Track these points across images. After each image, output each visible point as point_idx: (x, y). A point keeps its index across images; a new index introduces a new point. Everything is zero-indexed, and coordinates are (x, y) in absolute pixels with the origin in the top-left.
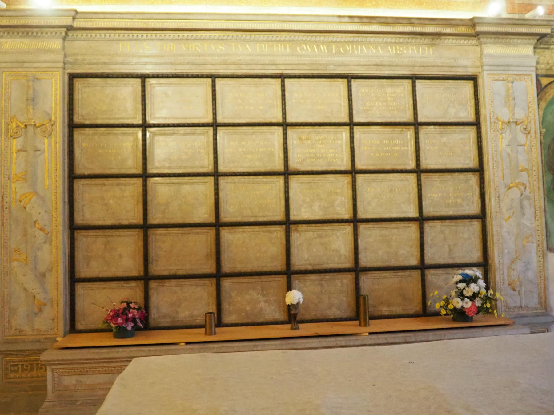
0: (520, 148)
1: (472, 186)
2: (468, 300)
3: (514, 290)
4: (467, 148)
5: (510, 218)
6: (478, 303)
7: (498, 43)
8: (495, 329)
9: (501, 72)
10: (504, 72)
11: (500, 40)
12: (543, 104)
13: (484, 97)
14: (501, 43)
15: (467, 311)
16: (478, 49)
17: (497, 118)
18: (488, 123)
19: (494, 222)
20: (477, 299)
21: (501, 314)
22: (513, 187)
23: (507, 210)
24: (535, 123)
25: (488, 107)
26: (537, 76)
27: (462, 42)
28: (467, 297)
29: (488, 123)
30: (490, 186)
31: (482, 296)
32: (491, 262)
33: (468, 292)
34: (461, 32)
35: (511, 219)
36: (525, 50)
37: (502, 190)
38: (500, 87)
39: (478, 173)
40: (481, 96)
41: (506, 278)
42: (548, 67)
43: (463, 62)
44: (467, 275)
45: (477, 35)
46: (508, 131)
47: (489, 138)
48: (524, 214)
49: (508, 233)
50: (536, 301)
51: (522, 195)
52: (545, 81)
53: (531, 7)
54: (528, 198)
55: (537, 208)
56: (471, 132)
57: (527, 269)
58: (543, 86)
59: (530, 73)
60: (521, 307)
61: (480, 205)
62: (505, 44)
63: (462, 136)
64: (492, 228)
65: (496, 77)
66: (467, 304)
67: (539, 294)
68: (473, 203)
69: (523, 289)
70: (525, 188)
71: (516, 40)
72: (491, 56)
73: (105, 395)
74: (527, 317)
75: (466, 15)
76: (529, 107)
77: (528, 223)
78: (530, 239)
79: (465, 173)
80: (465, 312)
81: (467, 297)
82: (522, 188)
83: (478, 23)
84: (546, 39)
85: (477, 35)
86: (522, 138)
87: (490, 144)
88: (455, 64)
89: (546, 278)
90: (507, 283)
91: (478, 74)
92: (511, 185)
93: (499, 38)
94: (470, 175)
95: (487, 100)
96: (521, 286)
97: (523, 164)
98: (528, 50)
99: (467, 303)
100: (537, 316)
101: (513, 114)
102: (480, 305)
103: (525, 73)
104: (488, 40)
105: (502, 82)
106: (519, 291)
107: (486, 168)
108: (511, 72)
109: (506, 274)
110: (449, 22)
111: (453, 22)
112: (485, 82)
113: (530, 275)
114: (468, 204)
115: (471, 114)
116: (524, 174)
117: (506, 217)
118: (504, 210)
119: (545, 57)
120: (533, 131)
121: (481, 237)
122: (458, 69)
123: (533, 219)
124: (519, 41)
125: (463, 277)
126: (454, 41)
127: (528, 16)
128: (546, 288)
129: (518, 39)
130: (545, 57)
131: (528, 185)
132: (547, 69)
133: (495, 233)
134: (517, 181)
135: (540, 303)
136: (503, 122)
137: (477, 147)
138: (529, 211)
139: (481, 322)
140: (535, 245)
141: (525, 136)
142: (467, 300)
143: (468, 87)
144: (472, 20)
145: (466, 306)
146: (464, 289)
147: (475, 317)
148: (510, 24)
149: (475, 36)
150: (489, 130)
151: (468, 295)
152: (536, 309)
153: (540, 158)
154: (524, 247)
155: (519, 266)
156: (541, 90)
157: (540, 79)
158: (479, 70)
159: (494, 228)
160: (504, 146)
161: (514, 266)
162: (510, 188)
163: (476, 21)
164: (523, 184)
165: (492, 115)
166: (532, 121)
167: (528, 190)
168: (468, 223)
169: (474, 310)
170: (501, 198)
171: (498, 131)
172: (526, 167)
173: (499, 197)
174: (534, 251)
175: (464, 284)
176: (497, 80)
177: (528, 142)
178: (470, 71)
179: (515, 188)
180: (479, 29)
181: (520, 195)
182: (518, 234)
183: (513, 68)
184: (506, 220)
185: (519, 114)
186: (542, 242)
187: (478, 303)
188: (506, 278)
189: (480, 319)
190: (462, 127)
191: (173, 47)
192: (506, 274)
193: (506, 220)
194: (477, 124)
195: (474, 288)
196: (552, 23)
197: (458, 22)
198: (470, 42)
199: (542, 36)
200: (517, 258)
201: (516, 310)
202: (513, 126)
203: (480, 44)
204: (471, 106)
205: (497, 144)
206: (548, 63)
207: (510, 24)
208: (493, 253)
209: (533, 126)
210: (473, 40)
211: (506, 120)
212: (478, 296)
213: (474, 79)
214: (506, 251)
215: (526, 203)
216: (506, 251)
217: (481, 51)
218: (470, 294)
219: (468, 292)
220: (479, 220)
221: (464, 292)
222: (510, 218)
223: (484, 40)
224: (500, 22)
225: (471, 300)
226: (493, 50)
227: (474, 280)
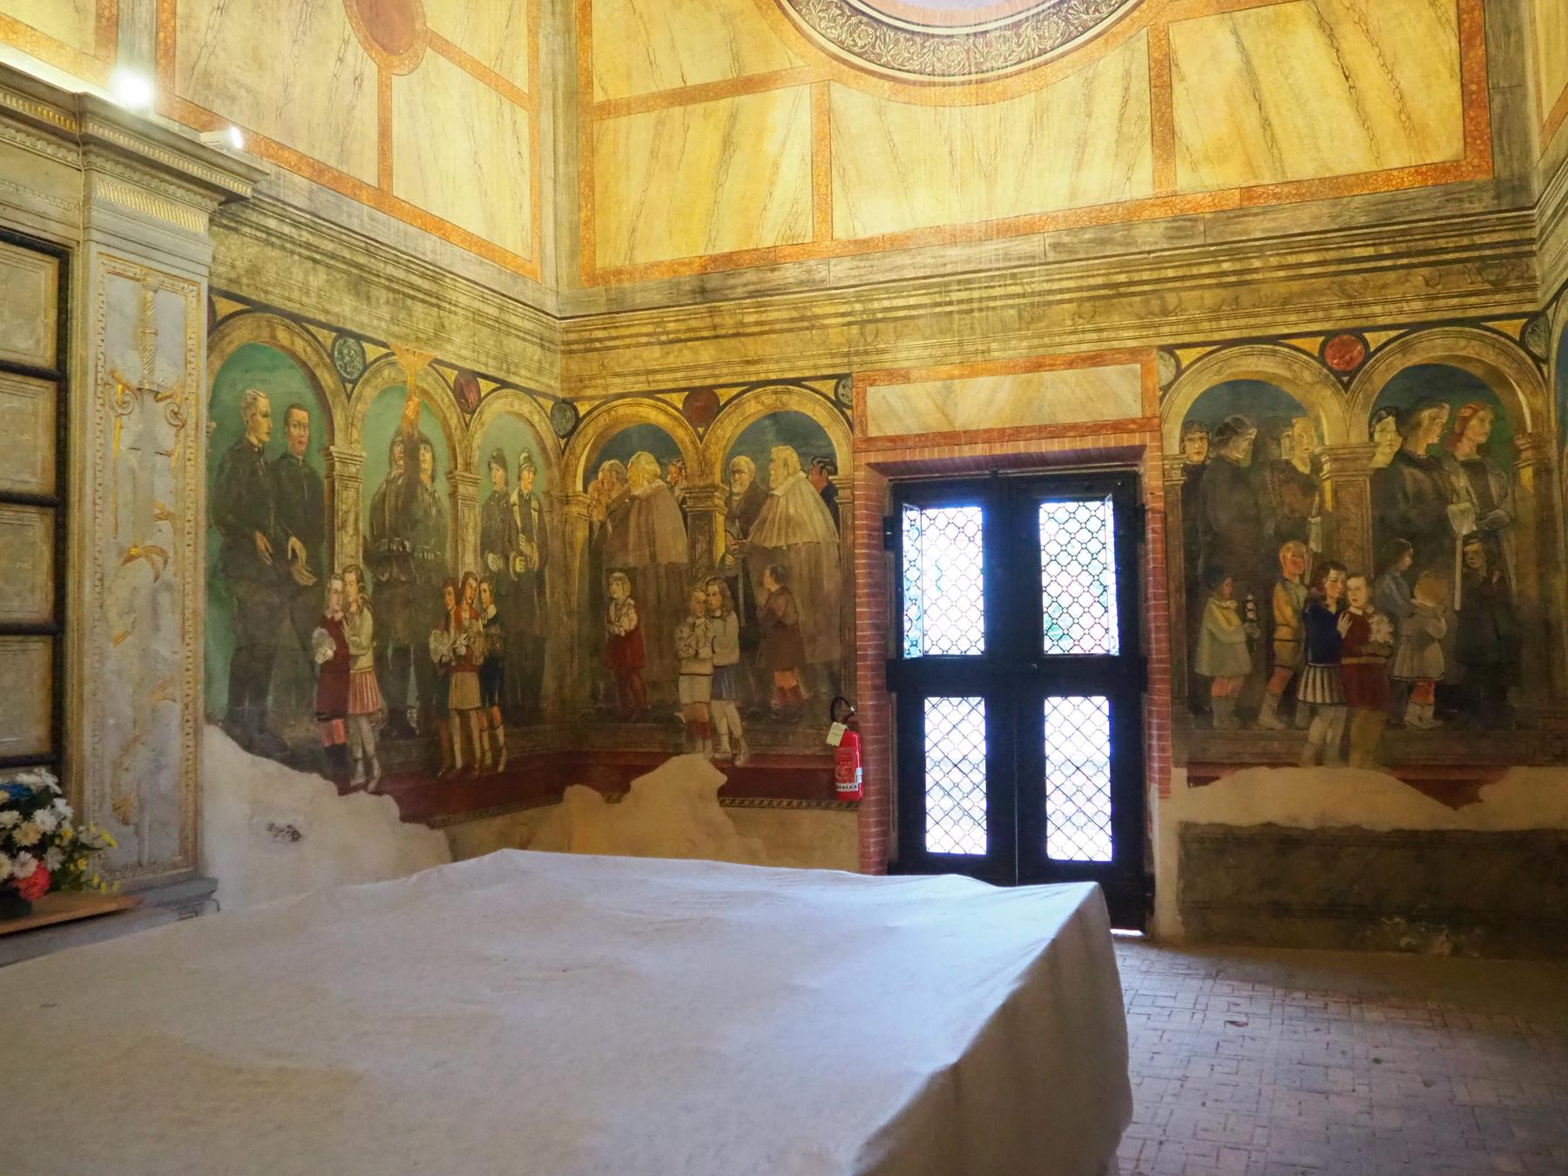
0: (160, 460)
1: (34, 543)
2: (29, 856)
3: (126, 822)
4: (26, 437)
5: (124, 636)
6: (53, 860)
7: (129, 180)
8: (97, 924)
9: (133, 257)
10: (139, 260)
11: (136, 177)
12: (218, 364)
13: (85, 306)
14: (136, 183)
15: (22, 886)
16: (80, 179)
17: (112, 373)
18: (91, 380)
19: (86, 645)
20: (52, 851)
21: (103, 887)
22: (139, 556)
23: (120, 616)
24: (197, 404)
25: (94, 339)
26: (211, 289)
27: (40, 145)
28: (26, 849)
29: (91, 380)
30: (82, 549)
31: (66, 842)
32: (72, 751)
33: (26, 835)
34: (45, 119)
35: (129, 638)
36: (189, 220)
37: (112, 562)
38: (122, 290)
39: (51, 511)
40: (76, 304)
41: (108, 791)
42: (233, 275)
43: (39, 202)
44: (26, 789)
45: (85, 143)
46: (137, 410)
47: (89, 425)
48: (157, 628)
49: (119, 674)
50: (175, 844)
51: (156, 579)
52: (225, 307)
53: (212, 121)
54: (169, 587)
55: (188, 613)
56: (41, 397)
57: (159, 768)
58: (219, 318)
59: (197, 278)
60: (140, 864)
61: (51, 598)
62: (148, 188)
63: (16, 403)
64: (81, 662)
65: (120, 267)
66: (27, 867)
67: (182, 829)
68: (32, 591)
69: (147, 818)
70: (166, 562)
71: (172, 189)
72: (111, 208)
73: (664, 757)
74: (152, 888)
75: (71, 84)
76: (187, 362)
77: (164, 651)
78: (169, 690)
79: (17, 507)
80: (17, 890)
81: (26, 849)
82: (159, 560)
83: (93, 113)
84: (234, 207)
85: (85, 143)
86: (166, 435)
87: (89, 436)
88: (15, 201)
89: (198, 788)
90: (108, 805)
91: (73, 244)
92: (134, 551)
93: (135, 170)
94: (31, 515)
95: (92, 320)
96: (141, 810)
97: (166, 502)
98: (197, 222)
99: (23, 865)
100: (175, 882)
101: (152, 371)
102: (57, 866)
103: (185, 275)
104: (109, 166)
105: (131, 282)
106: (137, 825)
107: (74, 498)
108: (154, 265)
109: (108, 781)
110: (16, 81)
111: (25, 84)
112: (92, 267)
113: (165, 781)
114: (18, 594)
115: (46, 347)
116: (165, 525)
117: (118, 630)
118: (112, 614)
119: (228, 249)
120: (191, 423)
121: (49, 683)
122: (22, 217)
123: (178, 641)
124: (180, 192)
125: (12, 794)
126: (20, 137)
127: (205, 138)
128: (198, 812)
129: (180, 187)
130: (228, 249)
131: (171, 554)
132: (230, 280)
133: (87, 672)
134: (149, 543)
135: (183, 851)
136: (126, 387)
137: (53, 437)
138: (170, 621)
139: (53, 912)
140: (178, 707)
141: (174, 430)
142: (25, 856)
143: (43, 273)
144: (80, 98)
145: (21, 873)
146: (16, 826)
147: (37, 904)
148: (172, 147)
149: (77, 144)
150: (90, 399)
151: (26, 842)
152: (175, 866)
153: (202, 492)
154: (154, 710)
155: (140, 760)
156: (216, 325)
157: (215, 298)
158: (77, 234)
159: (86, 660)
160: (123, 448)
161: (127, 762)
162: (131, 558)
163: (90, 106)
164: (162, 551)
165: (100, 363)
166: (192, 398)
167: (171, 568)
168: (16, 647)
169: (43, 881)
170: (107, 583)
171: (112, 408)
172: (172, 510)
173: (101, 580)
174: (176, 722)
175: (15, 814)
176: (118, 274)
177: (179, 449)
178: (54, 232)
179: (142, 559)
180: (93, 129)
181: (152, 578)
182: (142, 679)
183: (160, 256)
184: (117, 642)
185: (165, 375)
186: (196, 698)
187: (53, 860)
188: (108, 791)
189: (51, 909)
190: (19, 378)
191: (909, 349)
192: (108, 781)
193: (117, 642)
194: (58, 376)
195: (44, 819)
196: (257, 176)
197: (41, 90)
198: (62, 153)
199: (232, 198)
200: (135, 740)
201: (129, 874)
202: (149, 399)
203: (88, 169)
204: (46, 325)
205: (108, 441)
206: (233, 267)
207: (172, 147)
208: (80, 726)
209: (192, 410)
210: (69, 150)
211: (135, 383)
212: (52, 843)
213: (60, 254)
214: (111, 722)
215: (165, 599)
216: (111, 722)
217: (88, 185)
218: (33, 839)
219: (27, 835)
220: (44, 638)
221: (17, 835)
222: (124, 636)
223: (99, 162)
224: (144, 132)
225: (34, 856)
226: (116, 194)
227: (41, 799)
